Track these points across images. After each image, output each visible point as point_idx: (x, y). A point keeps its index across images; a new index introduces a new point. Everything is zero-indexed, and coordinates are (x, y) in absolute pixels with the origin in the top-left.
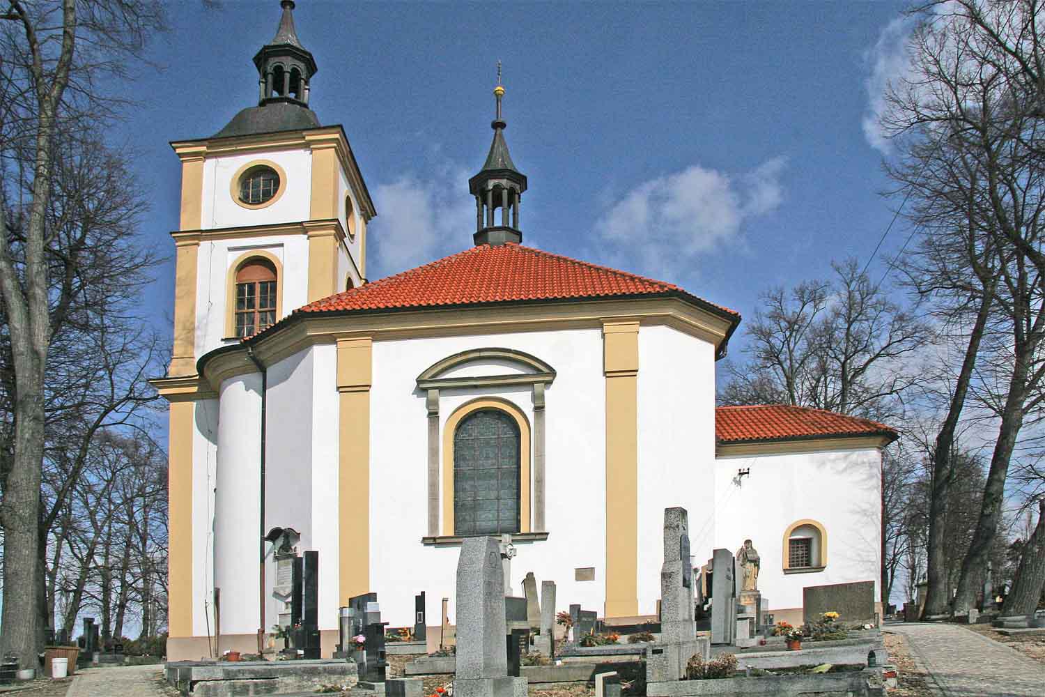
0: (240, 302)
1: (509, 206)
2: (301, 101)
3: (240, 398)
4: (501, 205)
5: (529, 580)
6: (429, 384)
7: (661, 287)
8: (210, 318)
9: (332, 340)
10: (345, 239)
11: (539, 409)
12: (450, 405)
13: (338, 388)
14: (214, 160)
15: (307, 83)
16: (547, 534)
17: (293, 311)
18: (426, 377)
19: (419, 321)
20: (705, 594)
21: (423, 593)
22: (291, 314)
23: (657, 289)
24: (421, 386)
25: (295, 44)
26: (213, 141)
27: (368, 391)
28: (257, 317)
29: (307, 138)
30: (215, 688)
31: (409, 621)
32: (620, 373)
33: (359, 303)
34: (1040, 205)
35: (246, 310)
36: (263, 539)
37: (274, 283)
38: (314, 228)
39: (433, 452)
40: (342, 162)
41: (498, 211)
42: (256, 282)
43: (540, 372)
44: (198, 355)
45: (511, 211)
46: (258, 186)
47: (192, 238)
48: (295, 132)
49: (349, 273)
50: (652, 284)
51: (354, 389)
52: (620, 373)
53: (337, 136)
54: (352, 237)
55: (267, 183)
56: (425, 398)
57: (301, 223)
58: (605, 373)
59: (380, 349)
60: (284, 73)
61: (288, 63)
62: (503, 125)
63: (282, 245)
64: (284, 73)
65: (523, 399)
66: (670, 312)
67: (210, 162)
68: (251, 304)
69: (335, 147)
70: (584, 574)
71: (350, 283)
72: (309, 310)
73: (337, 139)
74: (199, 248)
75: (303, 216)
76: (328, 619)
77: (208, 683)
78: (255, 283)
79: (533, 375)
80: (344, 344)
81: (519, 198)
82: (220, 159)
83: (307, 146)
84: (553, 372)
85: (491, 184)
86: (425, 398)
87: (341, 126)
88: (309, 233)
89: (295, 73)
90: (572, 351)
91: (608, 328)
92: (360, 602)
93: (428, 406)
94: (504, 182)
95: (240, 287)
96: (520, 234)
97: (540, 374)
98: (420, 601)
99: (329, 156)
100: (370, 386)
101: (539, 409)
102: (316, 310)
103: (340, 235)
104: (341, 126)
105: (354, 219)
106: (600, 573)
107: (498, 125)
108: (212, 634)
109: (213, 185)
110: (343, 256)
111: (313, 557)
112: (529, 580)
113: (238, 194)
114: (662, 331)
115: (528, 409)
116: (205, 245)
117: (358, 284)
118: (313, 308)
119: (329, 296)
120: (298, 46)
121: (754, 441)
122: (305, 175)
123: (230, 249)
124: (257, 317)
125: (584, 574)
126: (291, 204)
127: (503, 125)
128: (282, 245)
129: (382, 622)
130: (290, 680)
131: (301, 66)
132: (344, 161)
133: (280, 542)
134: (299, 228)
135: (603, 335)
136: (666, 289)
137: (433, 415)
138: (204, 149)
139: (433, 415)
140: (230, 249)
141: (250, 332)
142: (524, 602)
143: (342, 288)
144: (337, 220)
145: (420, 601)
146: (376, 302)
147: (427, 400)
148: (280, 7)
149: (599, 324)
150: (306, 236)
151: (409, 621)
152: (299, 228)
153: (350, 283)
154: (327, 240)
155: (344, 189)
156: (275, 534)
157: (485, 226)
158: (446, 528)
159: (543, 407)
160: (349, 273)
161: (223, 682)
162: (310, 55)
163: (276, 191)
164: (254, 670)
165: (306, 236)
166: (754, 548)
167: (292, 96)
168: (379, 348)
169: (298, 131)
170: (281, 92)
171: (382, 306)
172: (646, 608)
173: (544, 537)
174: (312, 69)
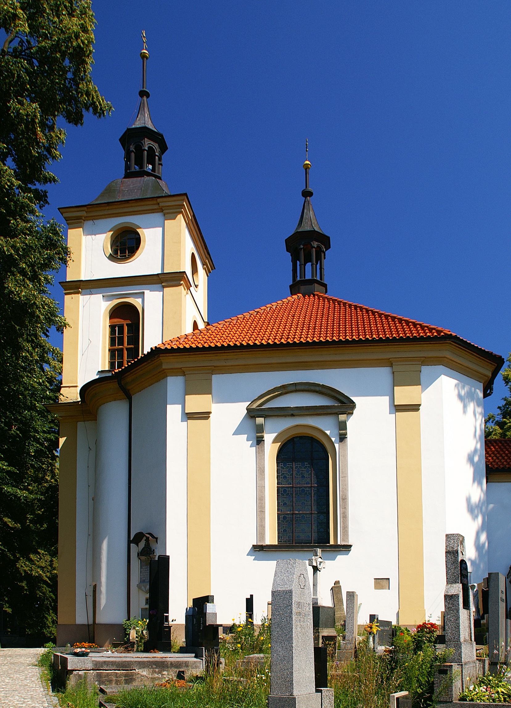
1: (317, 263)
4: (310, 261)
5: (336, 589)
7: (439, 332)
9: (181, 372)
10: (191, 288)
17: (151, 349)
20: (481, 612)
21: (252, 596)
22: (149, 350)
23: (435, 334)
29: (161, 204)
30: (85, 677)
31: (240, 618)
33: (202, 342)
36: (129, 542)
38: (166, 281)
39: (260, 471)
41: (309, 265)
43: (342, 402)
44: (80, 385)
45: (318, 266)
48: (162, 206)
49: (194, 316)
50: (431, 330)
60: (141, 149)
61: (147, 143)
62: (310, 194)
64: (141, 149)
65: (327, 427)
68: (121, 342)
70: (382, 583)
71: (195, 325)
76: (177, 613)
77: (80, 673)
81: (325, 255)
87: (186, 194)
92: (200, 604)
96: (325, 286)
98: (250, 602)
102: (169, 347)
106: (394, 583)
107: (307, 194)
108: (91, 622)
111: (165, 560)
112: (336, 589)
117: (201, 326)
125: (382, 583)
127: (310, 194)
129: (218, 623)
130: (144, 672)
131: (156, 146)
133: (142, 544)
136: (442, 334)
141: (120, 365)
142: (332, 611)
143: (189, 330)
145: (250, 602)
146: (214, 341)
151: (240, 618)
153: (195, 325)
156: (139, 537)
157: (298, 279)
158: (271, 537)
160: (194, 316)
161: (92, 671)
162: (162, 136)
164: (115, 662)
170: (141, 166)
171: (219, 345)
172: (434, 612)
174: (164, 148)
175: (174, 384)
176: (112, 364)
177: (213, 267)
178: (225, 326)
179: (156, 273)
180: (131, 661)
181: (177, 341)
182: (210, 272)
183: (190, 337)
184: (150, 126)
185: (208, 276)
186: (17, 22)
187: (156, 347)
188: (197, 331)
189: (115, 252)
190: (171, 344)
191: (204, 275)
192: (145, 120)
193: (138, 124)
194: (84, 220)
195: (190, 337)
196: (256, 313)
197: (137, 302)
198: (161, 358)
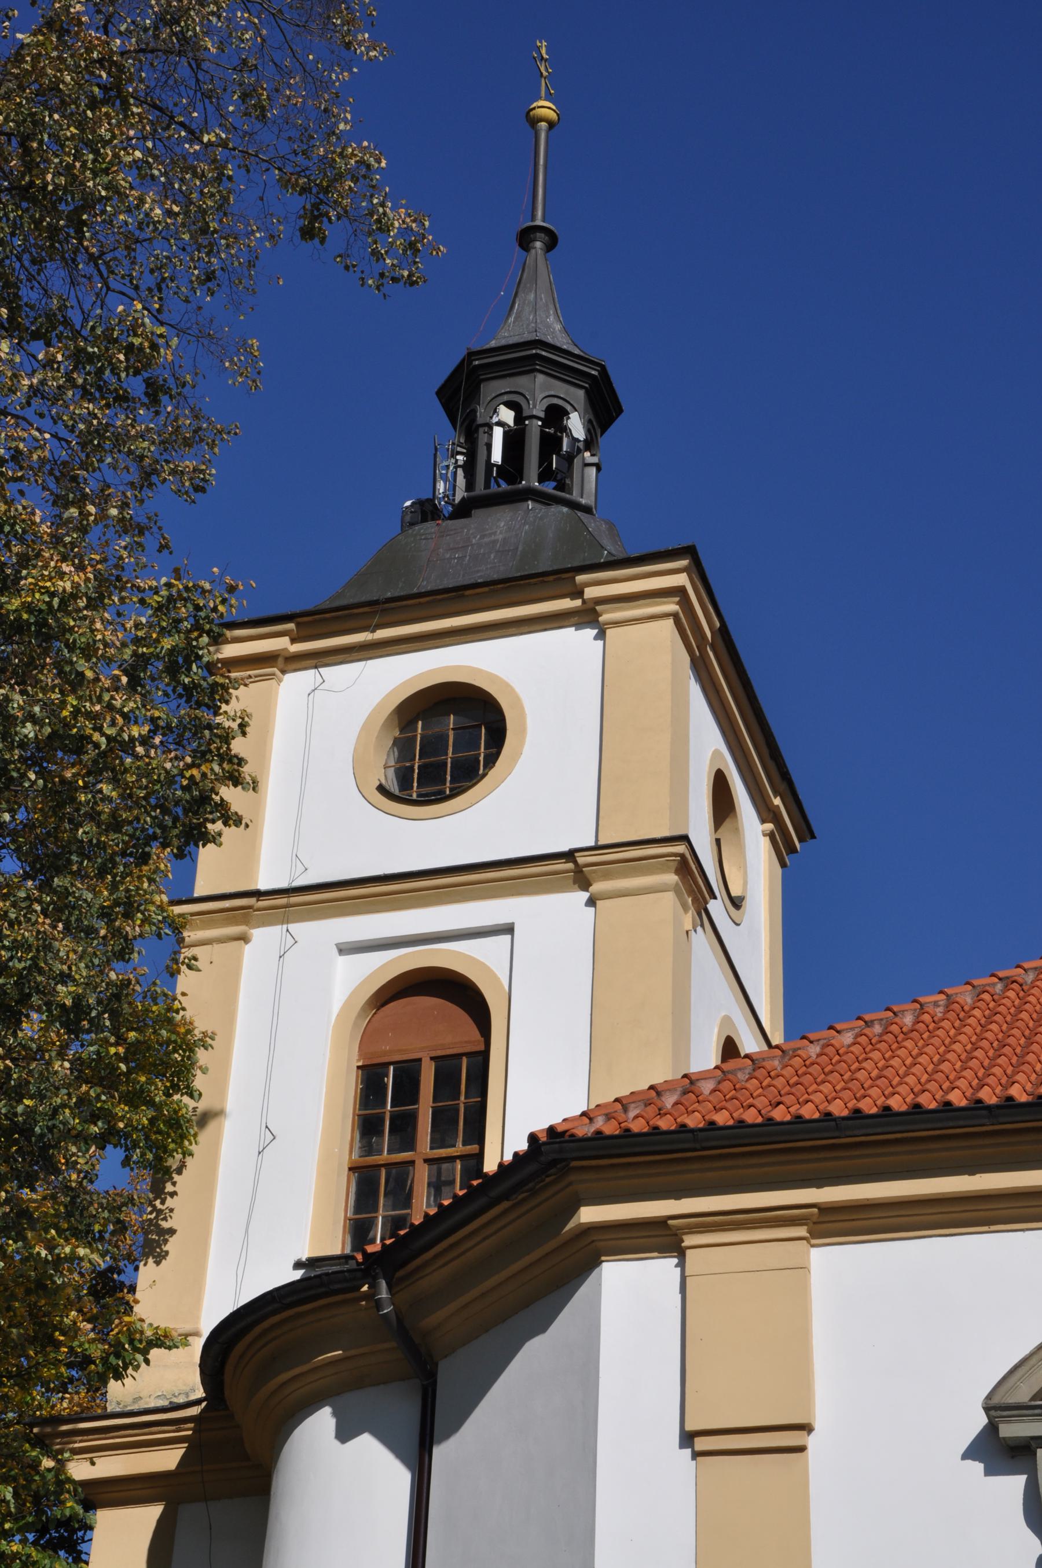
0: (368, 1127)
2: (575, 496)
8: (259, 1203)
9: (661, 1239)
14: (312, 671)
17: (533, 1138)
18: (1023, 1394)
19: (632, 608)
22: (523, 1146)
24: (1010, 1430)
25: (563, 341)
26: (312, 621)
27: (801, 1449)
28: (422, 1175)
34: (303, 171)
35: (385, 1157)
37: (481, 1062)
38: (610, 868)
40: (700, 667)
42: (425, 1052)
46: (447, 744)
49: (727, 1020)
51: (747, 1442)
53: (681, 580)
54: (736, 903)
55: (466, 738)
56: (1021, 1480)
57: (569, 855)
58: (687, 1438)
63: (509, 930)
67: (294, 685)
68: (404, 1129)
69: (675, 616)
71: (730, 1048)
72: (585, 1130)
74: (247, 948)
78: (420, 1060)
82: (297, 928)
83: (587, 616)
86: (1021, 1480)
88: (597, 887)
95: (371, 1078)
99: (655, 645)
100: (806, 1428)
103: (695, 885)
104: (690, 551)
105: (737, 831)
109: (312, 729)
110: (701, 940)
113: (381, 769)
116: (265, 937)
118: (599, 1123)
119: (657, 1079)
120: (582, 354)
122: (593, 701)
123: (346, 949)
124: (422, 1175)
126: (536, 796)
132: (703, 655)
134: (570, 869)
138: (281, 643)
143: (705, 1057)
144: (685, 839)
147: (1031, 1488)
148: (518, 248)
150: (585, 896)
152: (570, 869)
155: (707, 744)
160: (727, 1020)
163: (492, 760)
165: (585, 896)
167: (549, 487)
168: (836, 1269)
169: (559, 578)
171: (838, 1109)
175: (630, 1299)
176: (359, 1231)
177: (807, 832)
178: (863, 1040)
179: (565, 848)
180: (327, 1274)
181: (648, 1104)
182: (792, 850)
183: (707, 1087)
184: (554, 331)
185: (783, 865)
186: (81, 574)
187: (551, 1130)
188: (732, 1064)
189: (404, 777)
190: (622, 1117)
191: (769, 851)
192: (540, 316)
193: (510, 333)
194: (284, 672)
195: (707, 1087)
196: (999, 987)
197: (480, 960)
198: (572, 1177)
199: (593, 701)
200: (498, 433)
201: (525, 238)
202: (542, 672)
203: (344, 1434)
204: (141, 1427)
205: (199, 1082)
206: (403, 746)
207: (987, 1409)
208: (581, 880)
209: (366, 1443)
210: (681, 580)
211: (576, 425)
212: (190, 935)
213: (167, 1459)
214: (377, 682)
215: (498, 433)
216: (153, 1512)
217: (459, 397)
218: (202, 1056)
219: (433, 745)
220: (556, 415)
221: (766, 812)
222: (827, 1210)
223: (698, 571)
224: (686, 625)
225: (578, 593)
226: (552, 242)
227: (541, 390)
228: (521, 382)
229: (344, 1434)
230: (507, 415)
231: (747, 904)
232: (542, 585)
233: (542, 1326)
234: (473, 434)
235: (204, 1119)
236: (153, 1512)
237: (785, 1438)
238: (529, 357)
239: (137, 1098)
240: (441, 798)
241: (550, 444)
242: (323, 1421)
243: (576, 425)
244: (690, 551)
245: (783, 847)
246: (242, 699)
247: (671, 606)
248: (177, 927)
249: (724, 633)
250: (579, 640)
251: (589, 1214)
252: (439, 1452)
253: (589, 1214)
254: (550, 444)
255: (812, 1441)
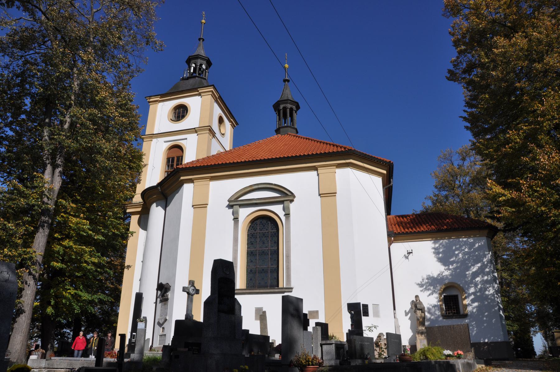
3: (157, 212)
6: (235, 203)
9: (191, 181)
11: (287, 215)
12: (245, 214)
13: (193, 206)
15: (296, 112)
16: (292, 288)
18: (233, 199)
26: (162, 96)
32: (327, 195)
37: (182, 157)
46: (180, 112)
47: (150, 137)
51: (200, 206)
52: (327, 195)
53: (212, 89)
55: (183, 112)
57: (194, 129)
58: (320, 195)
59: (213, 185)
63: (186, 139)
66: (352, 161)
67: (161, 104)
73: (212, 91)
75: (196, 125)
79: (284, 197)
80: (197, 183)
83: (199, 95)
84: (293, 195)
85: (282, 107)
87: (389, 167)
89: (291, 110)
90: (301, 182)
91: (320, 170)
93: (233, 214)
94: (289, 106)
95: (168, 159)
97: (285, 196)
99: (208, 98)
101: (287, 215)
109: (160, 114)
114: (349, 171)
115: (281, 214)
116: (154, 140)
121: (401, 234)
122: (200, 106)
123: (165, 142)
126: (192, 120)
128: (186, 139)
131: (294, 107)
135: (318, 175)
137: (236, 219)
139: (236, 219)
140: (165, 142)
149: (315, 169)
152: (195, 130)
154: (206, 135)
159: (289, 214)
166: (421, 301)
173: (290, 290)
174: (298, 107)
177: (237, 124)
193: (196, 54)
197: (182, 143)
199: (200, 106)
200: (192, 68)
201: (200, 39)
202: (194, 103)
203: (157, 206)
204: (136, 205)
205: (143, 160)
206: (175, 113)
207: (229, 201)
208: (196, 132)
209: (159, 207)
210: (212, 89)
211: (204, 67)
212: (145, 140)
213: (139, 209)
214: (170, 105)
215: (192, 68)
216: (139, 216)
217: (189, 62)
218: (144, 157)
219: (179, 113)
220: (201, 65)
221: (230, 121)
222: (212, 177)
223: (215, 88)
224: (213, 95)
225: (198, 91)
226: (203, 40)
227: (199, 61)
228: (196, 60)
229: (157, 206)
230: (194, 65)
231: (226, 135)
232: (193, 90)
233: (178, 193)
234: (190, 67)
235: (145, 165)
236: (139, 216)
237: (205, 206)
238: (197, 57)
239: (134, 163)
240: (179, 120)
241: (200, 69)
242: (154, 205)
243: (204, 67)
244: (213, 85)
245: (233, 126)
246: (152, 107)
247: (211, 93)
248: (143, 139)
249: (220, 97)
250: (198, 98)
251: (182, 178)
252: (167, 208)
253: (182, 178)
254: (200, 69)
255: (208, 206)
